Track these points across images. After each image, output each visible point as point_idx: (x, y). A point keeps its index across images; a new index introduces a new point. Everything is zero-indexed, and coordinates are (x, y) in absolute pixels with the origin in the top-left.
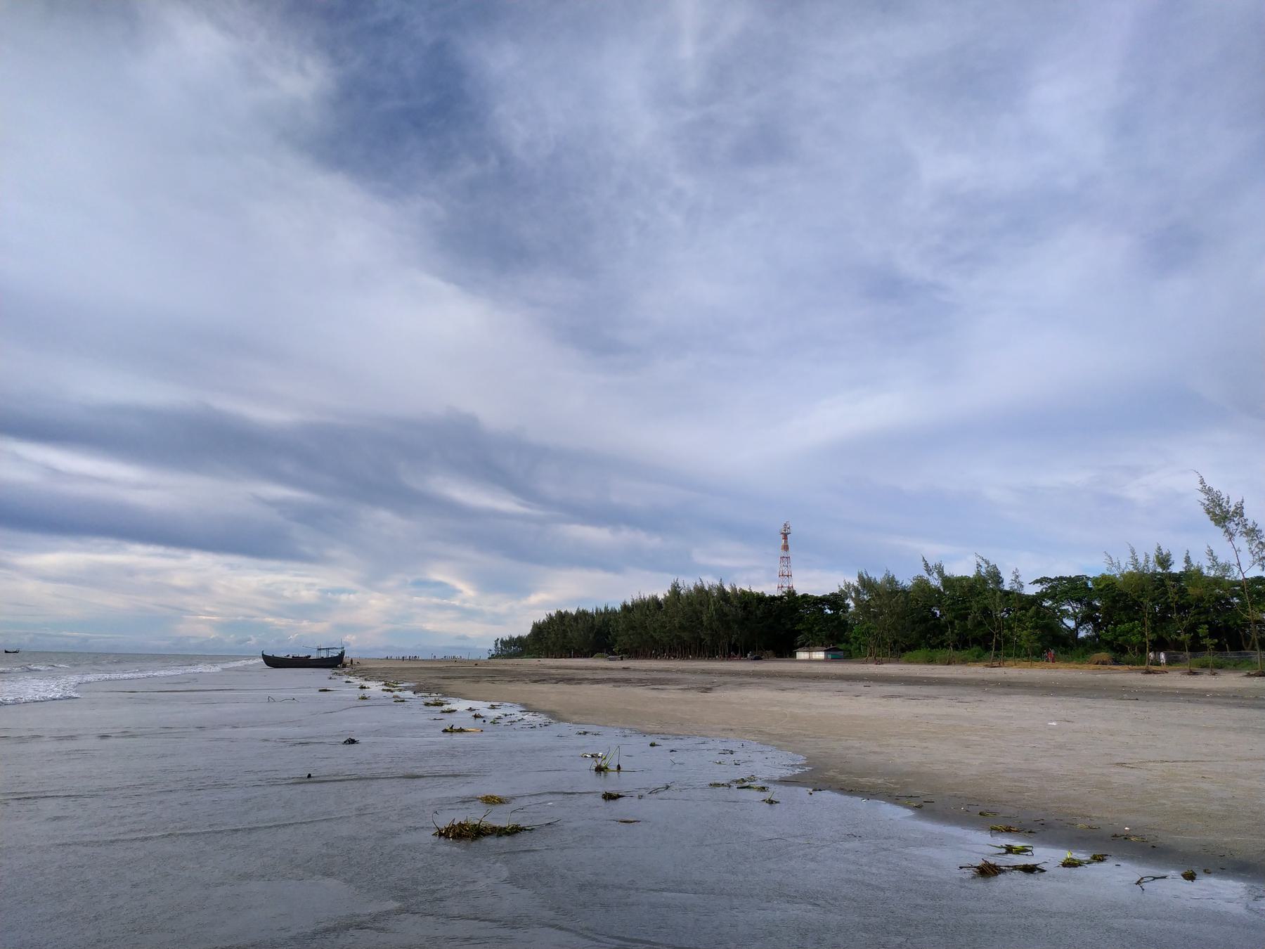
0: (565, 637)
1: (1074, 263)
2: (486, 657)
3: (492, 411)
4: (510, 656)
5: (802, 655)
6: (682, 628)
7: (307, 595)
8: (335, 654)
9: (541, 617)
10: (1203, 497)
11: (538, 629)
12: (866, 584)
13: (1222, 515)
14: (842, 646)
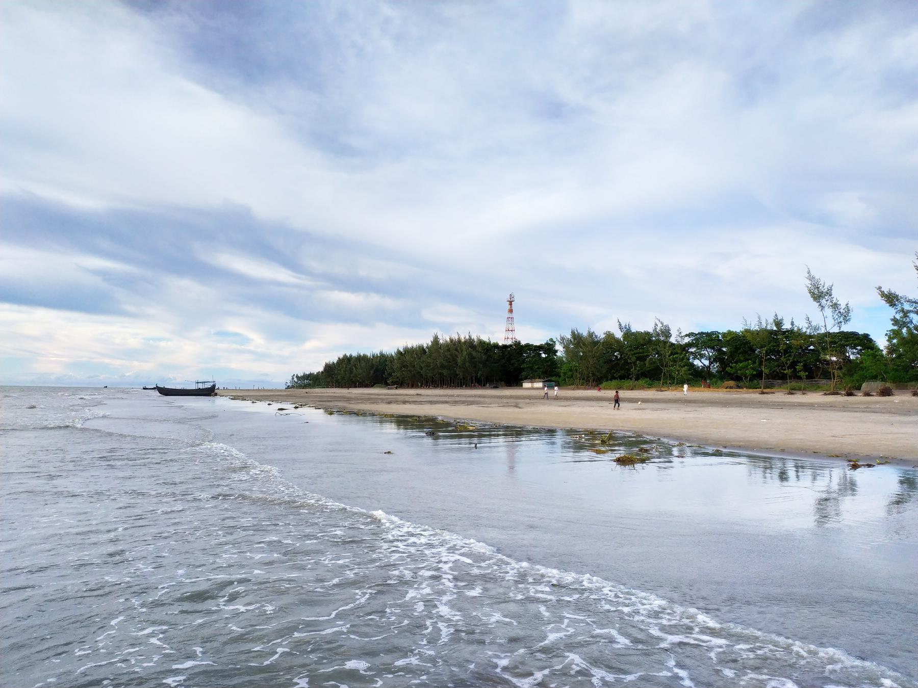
0: (351, 372)
1: (684, 93)
2: (284, 387)
3: (264, 203)
4: (305, 387)
5: (526, 385)
6: (442, 366)
7: (133, 343)
8: (208, 386)
9: (333, 358)
10: (808, 282)
11: (329, 368)
12: (577, 337)
13: (818, 294)
14: (553, 378)
